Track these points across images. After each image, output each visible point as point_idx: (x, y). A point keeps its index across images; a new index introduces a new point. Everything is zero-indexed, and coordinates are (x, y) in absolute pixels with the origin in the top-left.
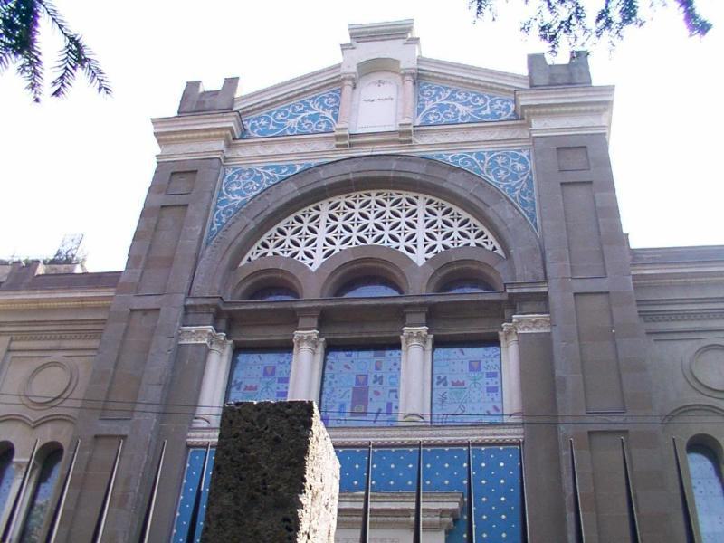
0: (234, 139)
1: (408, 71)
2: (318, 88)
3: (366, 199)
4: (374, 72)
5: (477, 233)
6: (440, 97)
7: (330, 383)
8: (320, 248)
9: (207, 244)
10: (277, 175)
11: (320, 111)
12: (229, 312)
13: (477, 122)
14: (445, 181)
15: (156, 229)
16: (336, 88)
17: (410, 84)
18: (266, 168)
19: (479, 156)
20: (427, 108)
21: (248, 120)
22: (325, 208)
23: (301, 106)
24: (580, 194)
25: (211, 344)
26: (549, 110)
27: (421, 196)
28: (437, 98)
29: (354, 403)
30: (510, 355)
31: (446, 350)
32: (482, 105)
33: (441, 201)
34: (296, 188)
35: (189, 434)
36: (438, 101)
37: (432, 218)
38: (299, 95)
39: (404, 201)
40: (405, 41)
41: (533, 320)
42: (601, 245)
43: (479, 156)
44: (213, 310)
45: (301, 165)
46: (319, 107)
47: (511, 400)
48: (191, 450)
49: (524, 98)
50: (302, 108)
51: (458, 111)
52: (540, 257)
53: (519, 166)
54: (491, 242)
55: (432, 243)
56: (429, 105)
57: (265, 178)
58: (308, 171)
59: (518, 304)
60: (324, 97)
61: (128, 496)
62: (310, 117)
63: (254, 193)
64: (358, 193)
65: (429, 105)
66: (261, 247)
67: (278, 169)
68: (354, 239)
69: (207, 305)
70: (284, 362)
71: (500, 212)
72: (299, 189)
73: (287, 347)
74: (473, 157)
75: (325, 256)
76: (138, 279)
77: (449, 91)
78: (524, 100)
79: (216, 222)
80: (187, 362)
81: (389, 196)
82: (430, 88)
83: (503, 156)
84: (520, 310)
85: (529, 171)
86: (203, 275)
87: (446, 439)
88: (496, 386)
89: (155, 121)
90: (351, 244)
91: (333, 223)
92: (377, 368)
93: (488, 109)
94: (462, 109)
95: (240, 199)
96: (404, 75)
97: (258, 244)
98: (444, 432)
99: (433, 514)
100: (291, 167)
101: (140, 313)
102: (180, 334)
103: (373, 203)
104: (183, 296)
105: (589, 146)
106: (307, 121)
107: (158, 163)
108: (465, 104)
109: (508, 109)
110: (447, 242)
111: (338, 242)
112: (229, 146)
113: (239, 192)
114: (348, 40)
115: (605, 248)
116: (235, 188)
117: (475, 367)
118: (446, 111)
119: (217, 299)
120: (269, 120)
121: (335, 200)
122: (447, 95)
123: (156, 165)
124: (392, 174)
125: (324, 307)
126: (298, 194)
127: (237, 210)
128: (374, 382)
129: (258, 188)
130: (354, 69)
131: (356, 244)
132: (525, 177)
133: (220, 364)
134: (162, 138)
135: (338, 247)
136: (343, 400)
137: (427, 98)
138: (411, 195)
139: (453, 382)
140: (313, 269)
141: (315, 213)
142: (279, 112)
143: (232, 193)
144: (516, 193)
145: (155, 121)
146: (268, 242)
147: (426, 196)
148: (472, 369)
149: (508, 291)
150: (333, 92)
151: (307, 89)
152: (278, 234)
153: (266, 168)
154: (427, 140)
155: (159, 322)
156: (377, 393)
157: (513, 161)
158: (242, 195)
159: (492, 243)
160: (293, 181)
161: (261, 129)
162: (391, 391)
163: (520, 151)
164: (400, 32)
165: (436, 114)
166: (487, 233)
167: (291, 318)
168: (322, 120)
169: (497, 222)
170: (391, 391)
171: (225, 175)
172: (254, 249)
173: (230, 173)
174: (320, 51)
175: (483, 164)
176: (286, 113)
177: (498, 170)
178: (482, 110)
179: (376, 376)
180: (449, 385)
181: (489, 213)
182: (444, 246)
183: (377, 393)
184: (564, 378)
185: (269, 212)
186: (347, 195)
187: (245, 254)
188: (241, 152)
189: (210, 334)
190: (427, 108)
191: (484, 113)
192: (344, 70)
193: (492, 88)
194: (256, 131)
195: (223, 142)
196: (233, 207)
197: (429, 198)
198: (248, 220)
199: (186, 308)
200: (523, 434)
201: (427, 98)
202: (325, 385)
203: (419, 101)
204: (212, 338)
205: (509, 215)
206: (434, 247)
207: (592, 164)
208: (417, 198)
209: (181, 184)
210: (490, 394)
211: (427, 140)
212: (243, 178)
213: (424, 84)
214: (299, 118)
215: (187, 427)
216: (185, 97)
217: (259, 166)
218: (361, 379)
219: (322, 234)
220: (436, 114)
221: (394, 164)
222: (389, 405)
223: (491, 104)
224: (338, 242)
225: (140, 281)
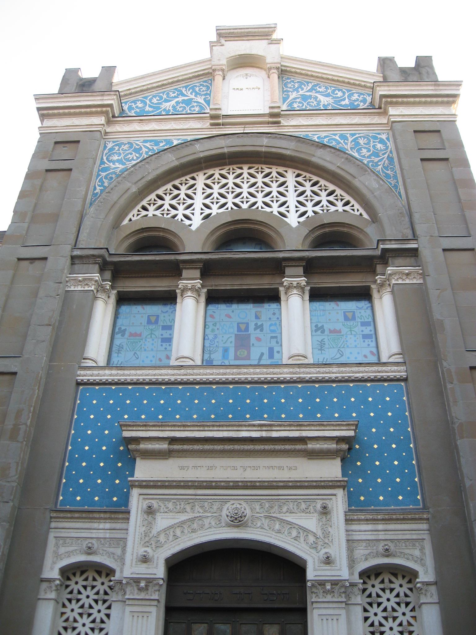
0: (114, 116)
1: (273, 65)
2: (190, 78)
3: (239, 171)
4: (241, 67)
5: (344, 201)
6: (302, 89)
7: (213, 330)
8: (197, 212)
9: (91, 204)
10: (155, 148)
11: (192, 96)
12: (114, 264)
13: (337, 110)
14: (314, 156)
15: (41, 190)
16: (206, 79)
17: (275, 77)
18: (145, 141)
19: (342, 136)
20: (291, 97)
21: (126, 103)
22: (201, 179)
23: (174, 93)
24: (437, 168)
25: (98, 291)
26: (405, 100)
27: (290, 171)
28: (300, 90)
29: (237, 348)
30: (384, 306)
31: (321, 303)
32: (341, 97)
33: (308, 175)
34: (174, 159)
35: (79, 372)
36: (301, 92)
37: (301, 189)
38: (172, 83)
39: (274, 174)
40: (269, 41)
41: (407, 271)
42: (462, 210)
43: (342, 136)
44: (99, 260)
45: (178, 139)
46: (191, 94)
47: (389, 343)
48: (81, 387)
49: (382, 88)
50: (176, 94)
51: (320, 101)
52: (407, 219)
53: (379, 146)
54: (357, 209)
55: (302, 209)
56: (293, 95)
57: (144, 150)
58: (185, 144)
59: (390, 259)
60: (196, 86)
61: (20, 429)
62: (183, 101)
63: (134, 162)
64: (231, 167)
65: (293, 95)
66: (141, 210)
67: (157, 143)
68: (230, 205)
69: (93, 256)
70: (167, 311)
71: (366, 183)
72: (177, 159)
73: (169, 298)
74: (337, 138)
75: (203, 219)
76: (24, 232)
77: (311, 85)
78: (382, 91)
79: (99, 186)
80: (75, 307)
81: (260, 169)
82: (293, 81)
83: (364, 138)
84: (393, 264)
85: (389, 149)
86: (88, 231)
87: (333, 376)
88: (378, 331)
89: (38, 98)
90: (227, 209)
91: (209, 191)
92: (257, 317)
93: (347, 100)
94: (324, 100)
95: (121, 167)
96: (270, 69)
97: (139, 207)
98: (331, 369)
99: (329, 442)
100: (168, 142)
101: (26, 263)
102: (67, 282)
103: (245, 175)
104: (69, 247)
105: (442, 131)
106: (181, 105)
107: (40, 134)
108: (328, 95)
109: (364, 101)
110: (317, 209)
111: (215, 207)
112: (109, 122)
113: (119, 161)
114: (214, 38)
115: (467, 213)
116: (116, 158)
117: (348, 317)
118: (309, 100)
119: (103, 250)
120: (145, 103)
121: (210, 172)
122: (309, 88)
123: (39, 136)
124: (264, 149)
125: (206, 259)
126: (176, 163)
127: (118, 176)
128: (255, 329)
129: (138, 158)
130: (224, 62)
131: (232, 208)
132: (386, 155)
133: (105, 310)
134: (45, 113)
135: (215, 210)
136: (226, 345)
137: (291, 90)
138: (281, 170)
139: (330, 330)
140: (193, 228)
141: (192, 182)
142: (155, 96)
143: (114, 162)
144: (380, 167)
145: (38, 98)
146: (148, 206)
147: (294, 170)
148: (346, 318)
149: (382, 246)
150: (203, 82)
151: (180, 78)
152: (157, 199)
153: (145, 141)
154: (294, 122)
155: (46, 270)
156: (259, 339)
157: (374, 142)
158: (123, 164)
159: (358, 210)
160: (170, 152)
161: (138, 110)
162: (272, 337)
163: (379, 134)
164: (264, 34)
165: (299, 103)
166: (353, 202)
167: (175, 270)
168: (196, 104)
169: (365, 191)
170: (272, 337)
171: (105, 147)
172: (135, 212)
173: (110, 145)
174: (193, 49)
175: (346, 144)
176: (161, 98)
177: (361, 149)
178: (341, 100)
179: (256, 324)
180: (327, 332)
181: (356, 183)
182: (313, 211)
183: (259, 339)
184: (442, 321)
185: (150, 178)
186: (220, 168)
187: (127, 215)
188: (117, 128)
189: (96, 281)
190: (291, 97)
191: (343, 103)
192: (215, 62)
193: (349, 83)
194: (133, 111)
195: (103, 118)
196: (115, 173)
197: (297, 172)
198: (129, 185)
199: (73, 258)
200: (406, 371)
201: (291, 90)
202: (208, 331)
203: (283, 92)
204: (101, 288)
205: (375, 185)
206: (305, 212)
207: (446, 144)
208: (286, 171)
209: (64, 152)
210: (366, 340)
211: (294, 122)
212: (122, 150)
213: (288, 78)
214: (173, 103)
215: (77, 366)
216: (65, 81)
217: (138, 141)
218: (243, 327)
219: (199, 200)
220: (299, 103)
221: (265, 141)
222: (271, 350)
223: (349, 96)
224: (215, 207)
225: (26, 233)
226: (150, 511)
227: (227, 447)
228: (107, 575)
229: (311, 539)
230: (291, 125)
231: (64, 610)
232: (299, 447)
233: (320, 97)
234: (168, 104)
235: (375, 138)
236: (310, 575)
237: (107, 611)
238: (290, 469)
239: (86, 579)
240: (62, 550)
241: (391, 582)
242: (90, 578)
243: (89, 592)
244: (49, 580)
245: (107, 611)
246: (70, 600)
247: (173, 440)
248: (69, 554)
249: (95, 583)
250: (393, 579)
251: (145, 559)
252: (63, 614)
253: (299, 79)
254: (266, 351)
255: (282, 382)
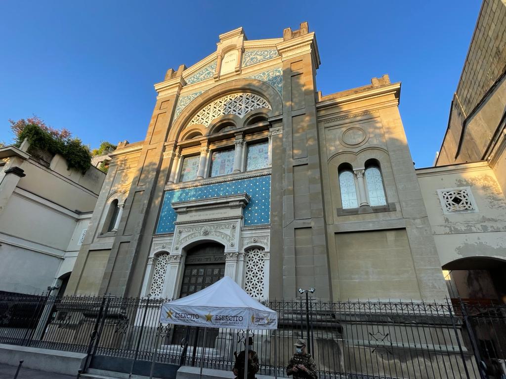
22: (212, 104)
36: (251, 57)
58: (207, 91)
67: (196, 94)
74: (261, 75)
121: (216, 101)
156: (228, 165)
172: (190, 124)
175: (264, 76)
183: (228, 165)
226: (180, 232)
227: (204, 208)
228: (262, 250)
229: (228, 238)
230: (245, 74)
231: (248, 264)
232: (227, 205)
233: (258, 57)
234: (201, 76)
235: (276, 71)
236: (226, 251)
237: (263, 264)
238: (224, 213)
239: (255, 252)
240: (156, 248)
241: (258, 252)
242: (256, 252)
243: (256, 257)
244: (151, 258)
245: (263, 264)
246: (249, 260)
247: (188, 207)
248: (157, 249)
249: (258, 253)
250: (259, 251)
251: (177, 249)
252: (247, 266)
253: (251, 50)
254: (230, 169)
255: (264, 175)
